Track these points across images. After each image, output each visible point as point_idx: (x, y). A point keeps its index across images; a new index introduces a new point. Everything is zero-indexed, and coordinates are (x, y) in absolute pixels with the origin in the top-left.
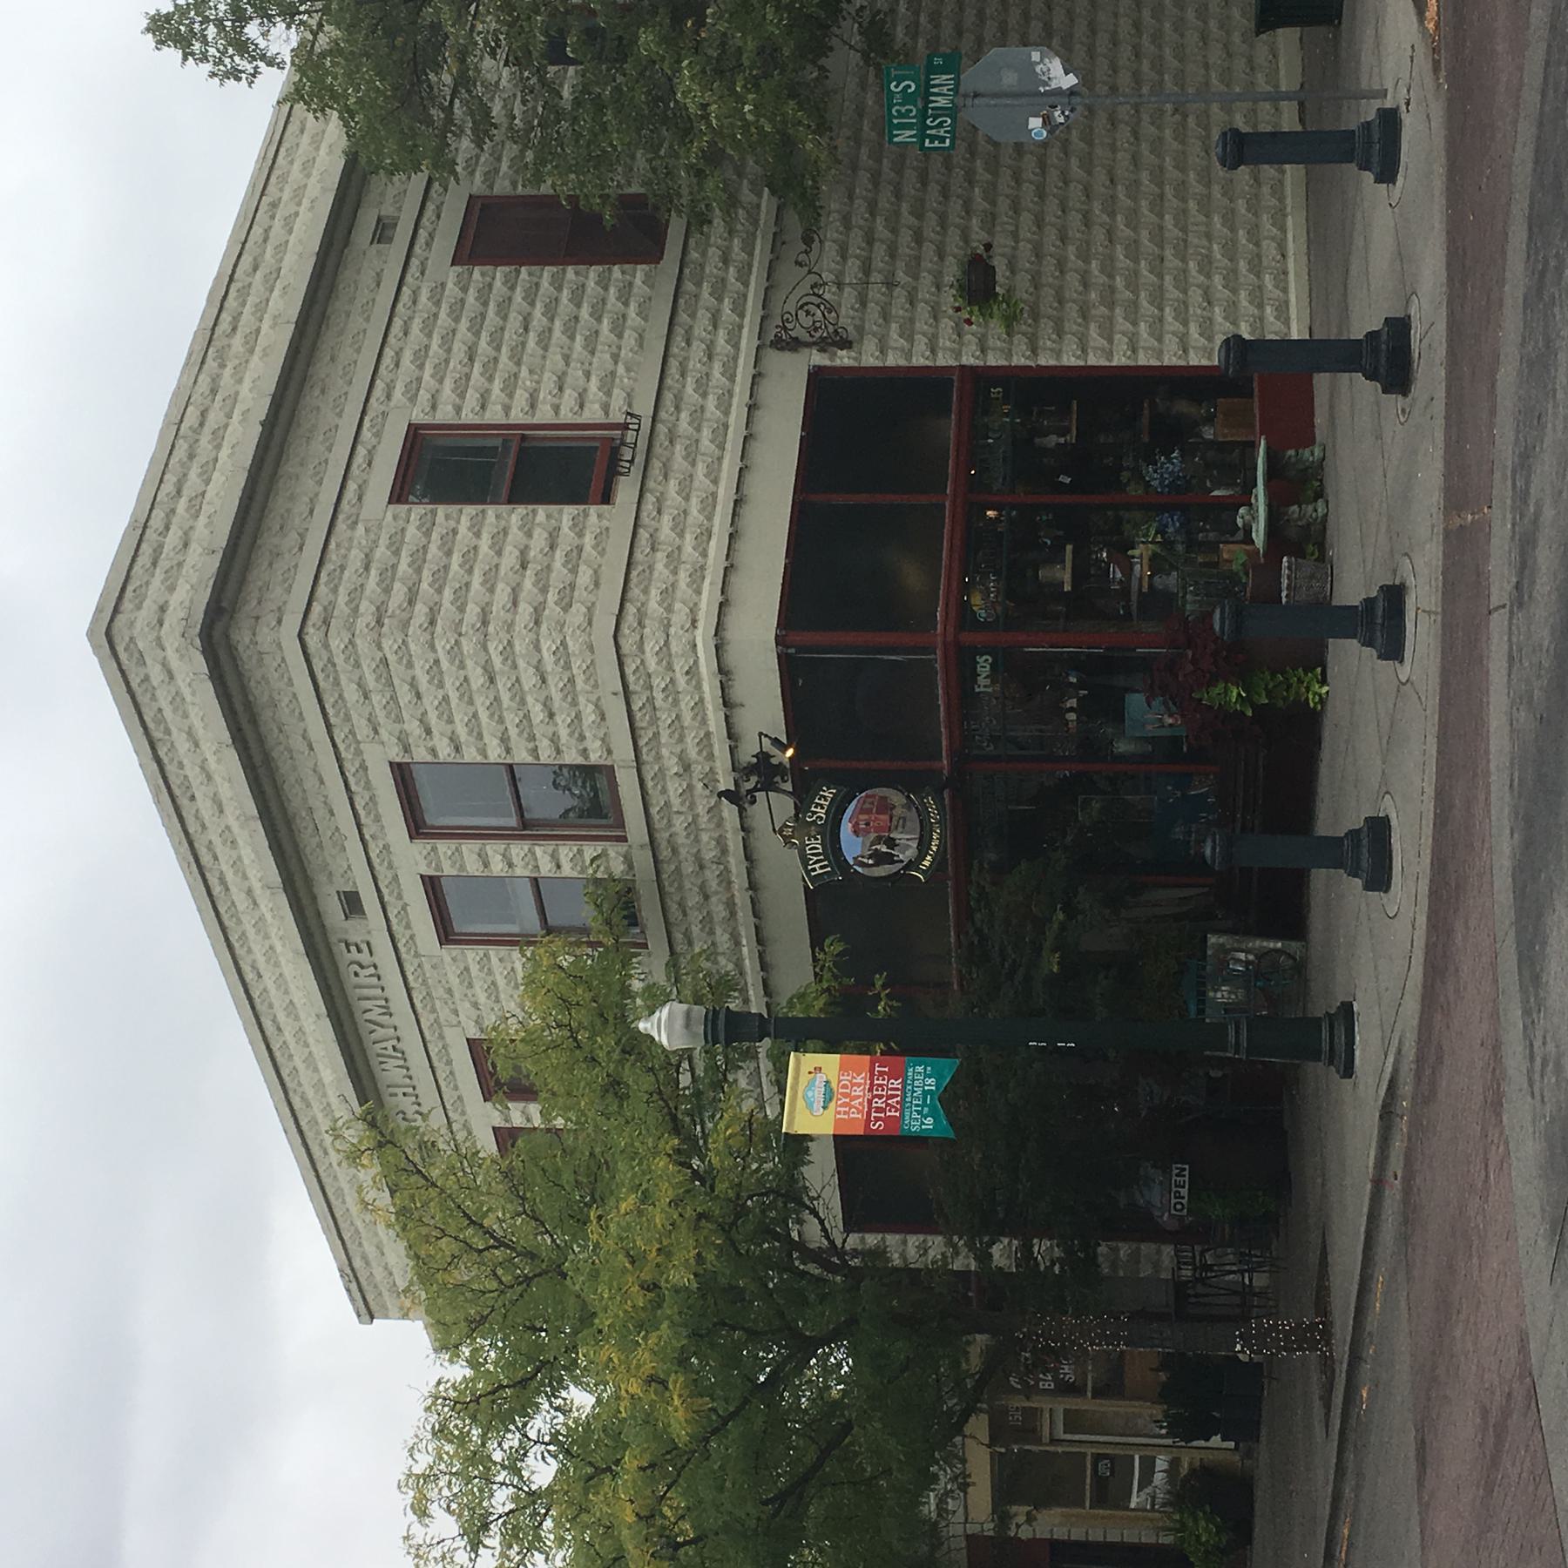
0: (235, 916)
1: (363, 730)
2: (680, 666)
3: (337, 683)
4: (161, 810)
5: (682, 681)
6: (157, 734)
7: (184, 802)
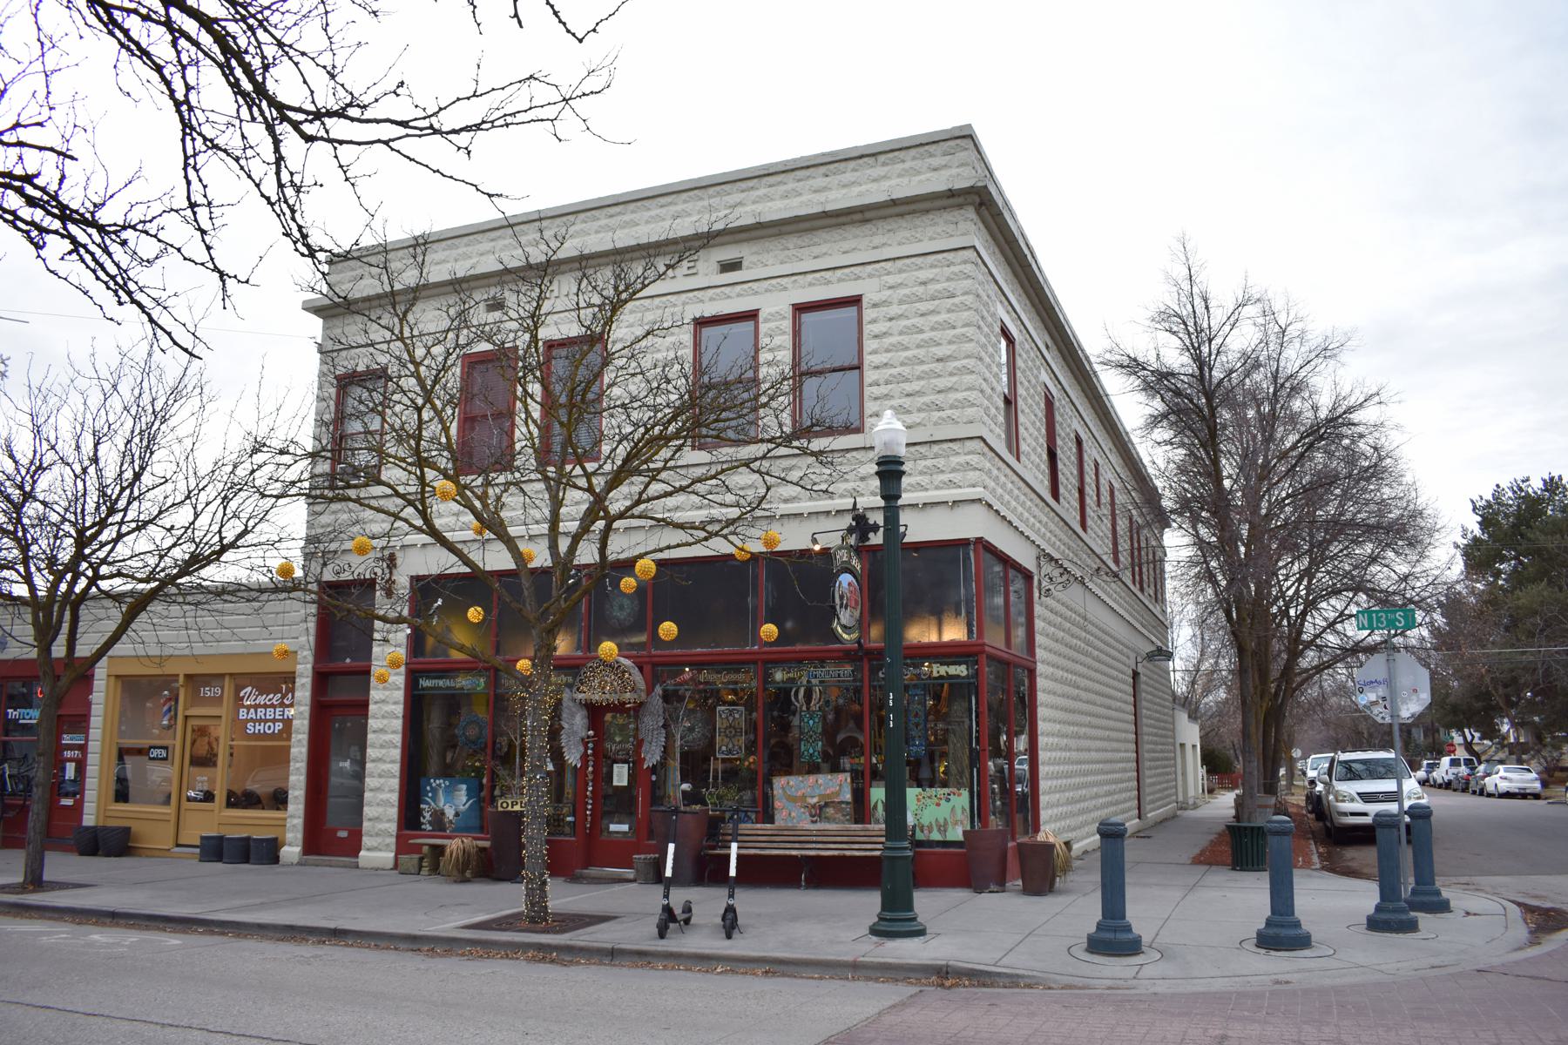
0: (450, 248)
1: (891, 280)
2: (956, 477)
3: (932, 266)
4: (816, 156)
5: (945, 477)
6: (882, 158)
7: (823, 170)
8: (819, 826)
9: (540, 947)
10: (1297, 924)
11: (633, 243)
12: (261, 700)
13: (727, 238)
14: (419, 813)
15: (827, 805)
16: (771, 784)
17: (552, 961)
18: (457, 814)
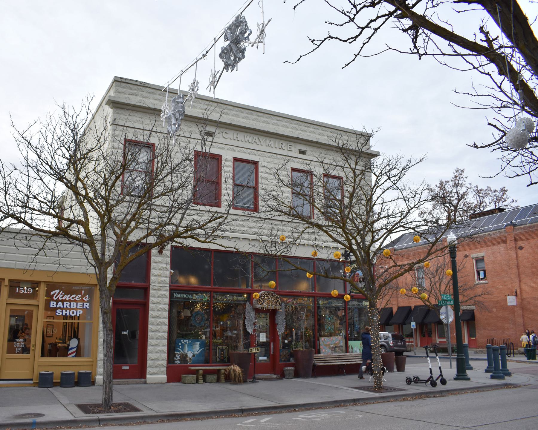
0: (297, 124)
7: (331, 130)
8: (334, 354)
9: (383, 398)
10: (508, 370)
11: (315, 140)
12: (67, 297)
13: (275, 136)
14: (175, 355)
15: (336, 347)
16: (319, 340)
17: (81, 427)
18: (194, 356)
